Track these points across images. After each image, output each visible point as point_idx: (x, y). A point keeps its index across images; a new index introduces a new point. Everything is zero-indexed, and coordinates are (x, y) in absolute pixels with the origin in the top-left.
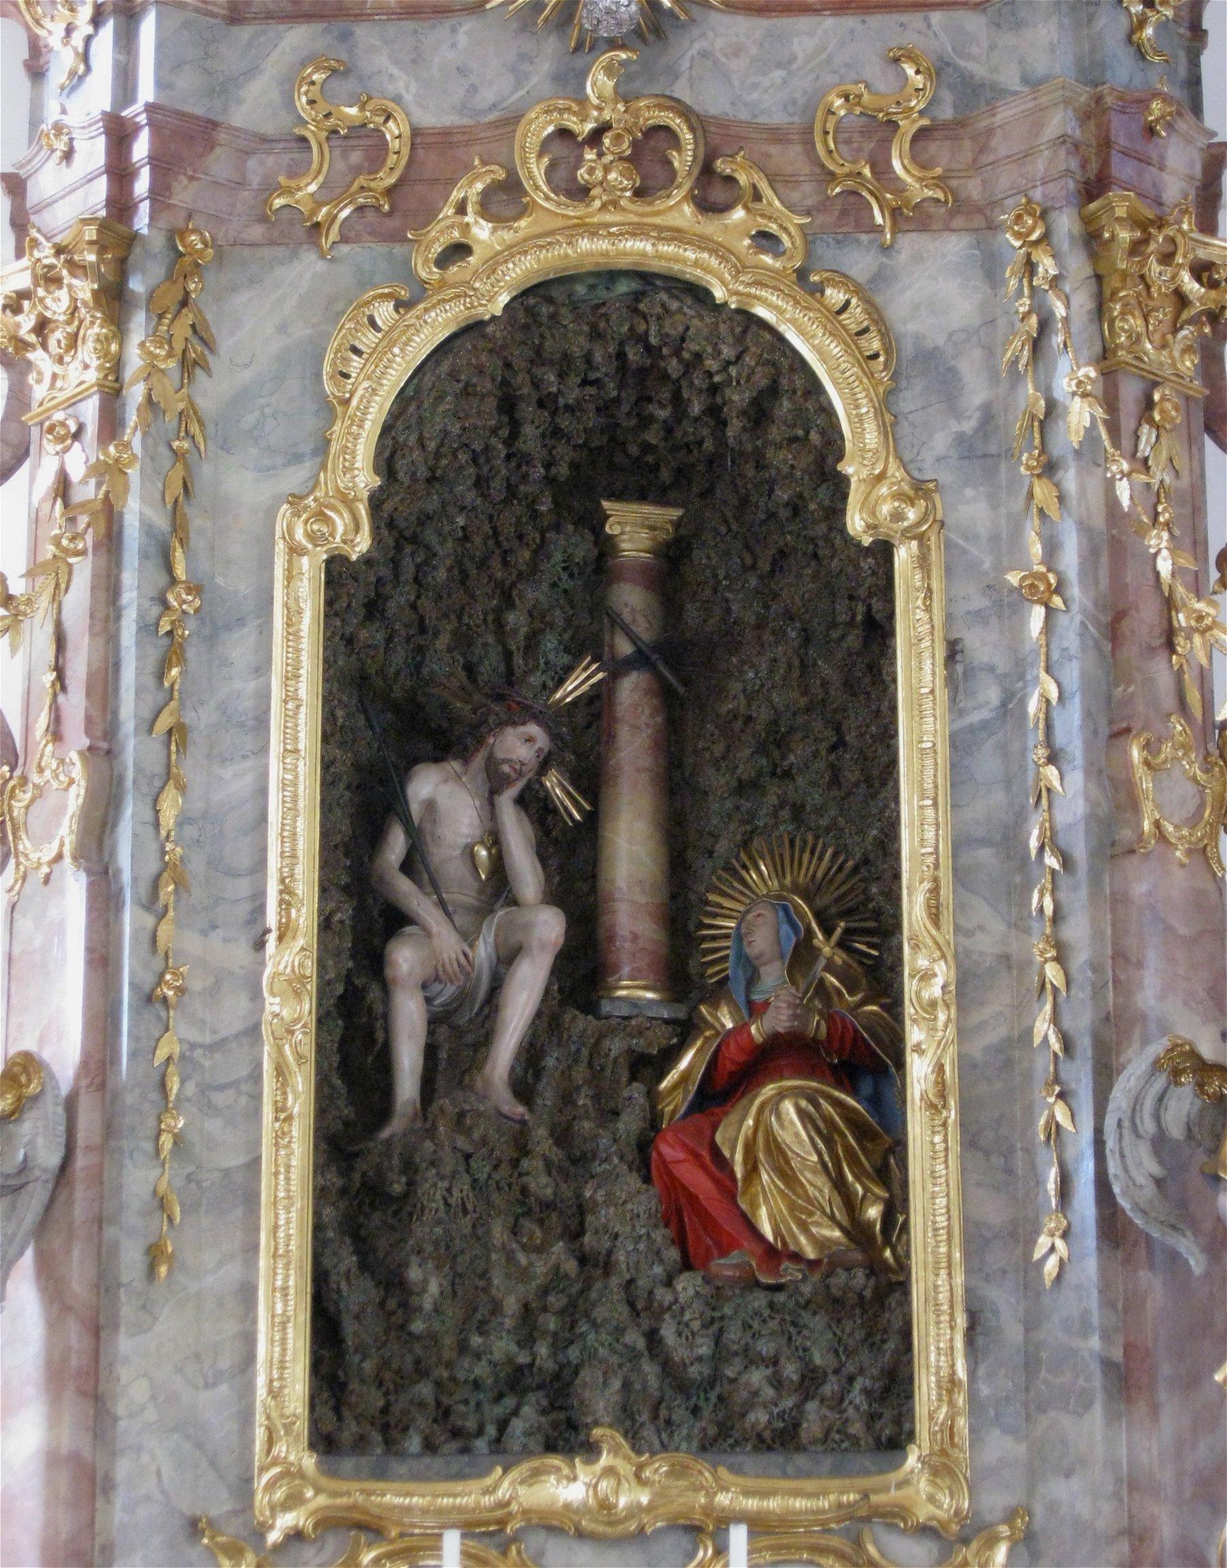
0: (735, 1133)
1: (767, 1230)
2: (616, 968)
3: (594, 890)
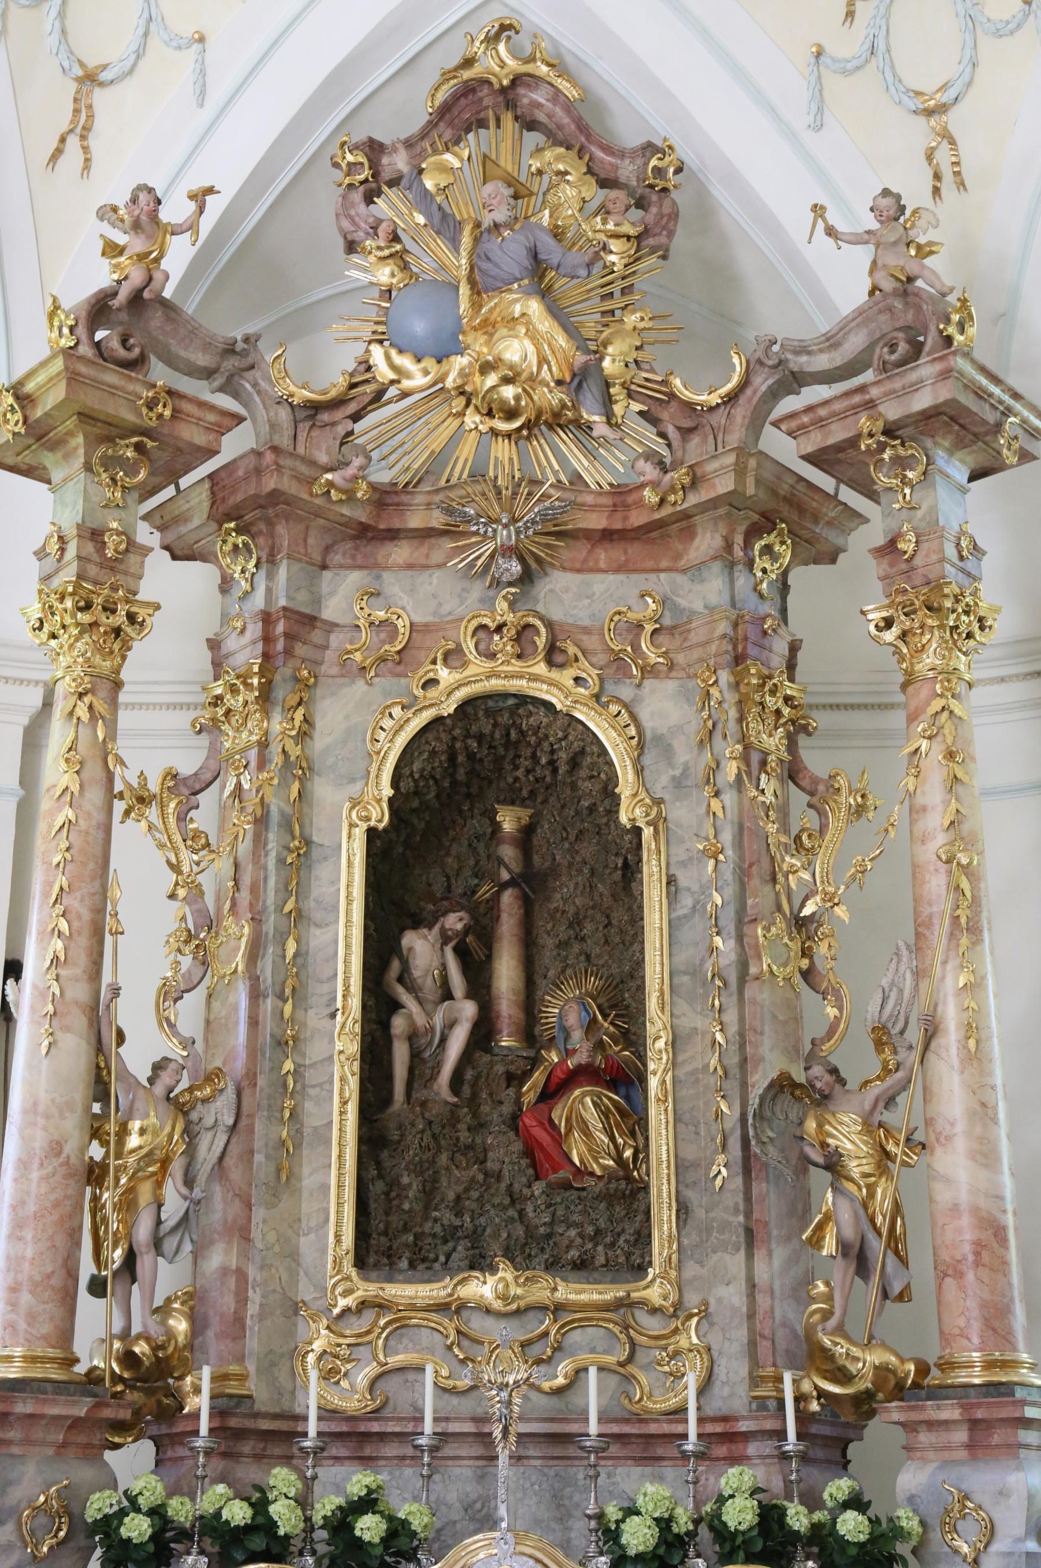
0: (559, 1114)
2: (501, 1032)
3: (489, 993)
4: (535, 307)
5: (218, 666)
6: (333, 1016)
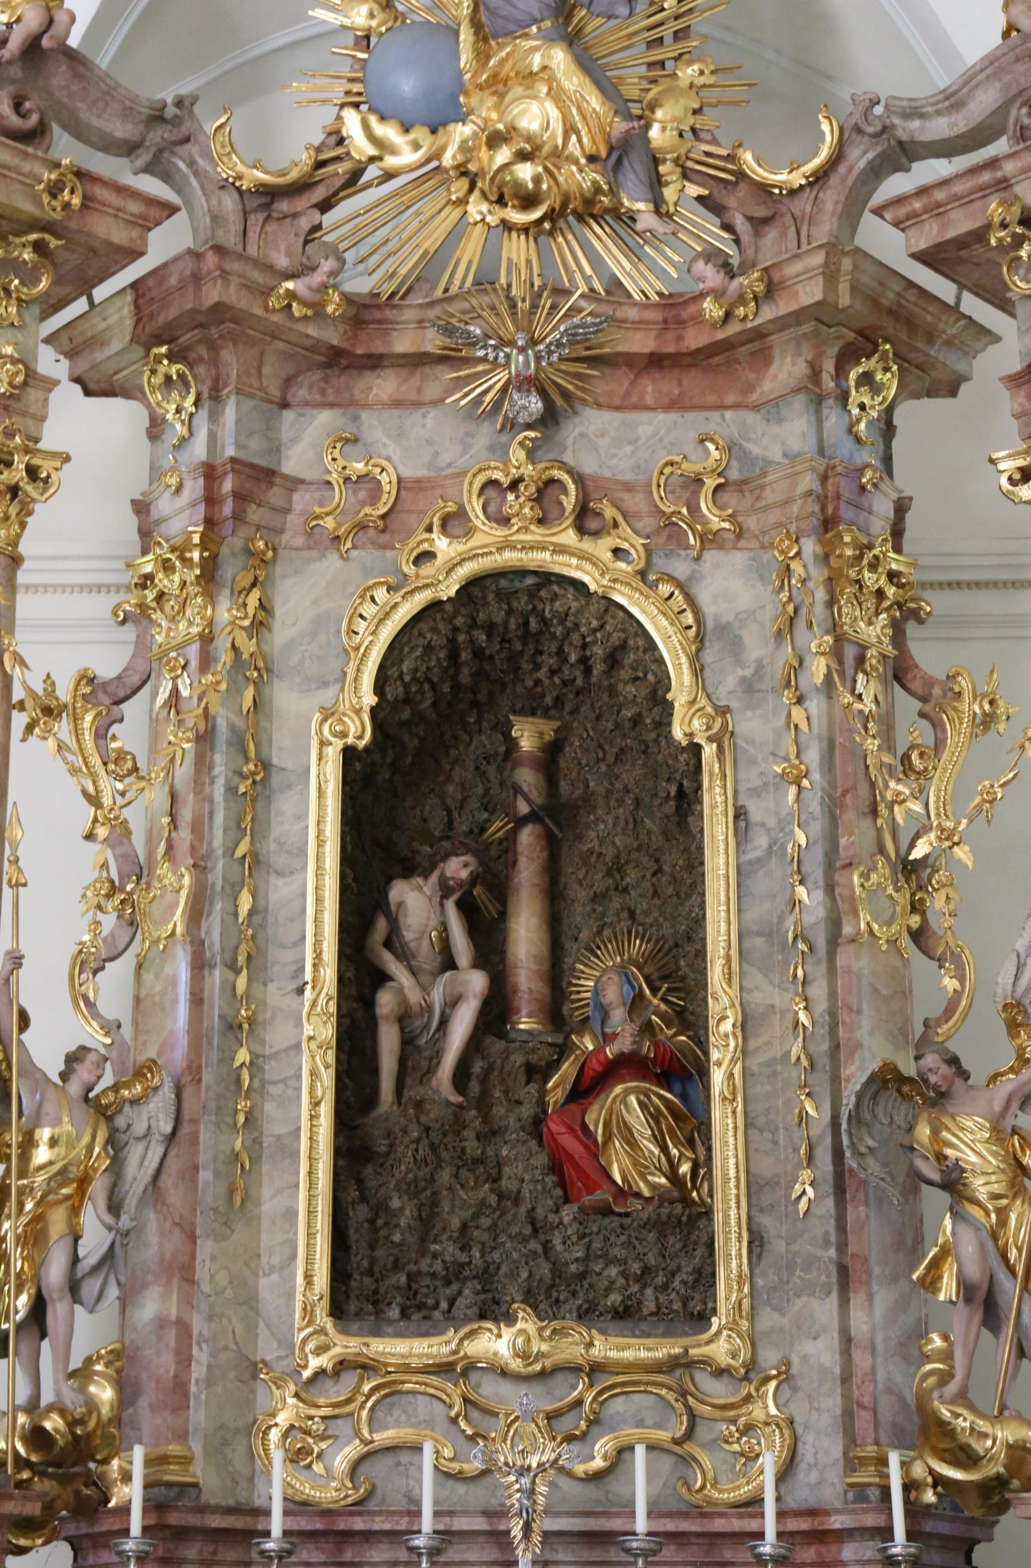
0: (595, 1118)
1: (618, 1178)
2: (518, 1011)
4: (559, 57)
5: (146, 536)
6: (300, 991)
